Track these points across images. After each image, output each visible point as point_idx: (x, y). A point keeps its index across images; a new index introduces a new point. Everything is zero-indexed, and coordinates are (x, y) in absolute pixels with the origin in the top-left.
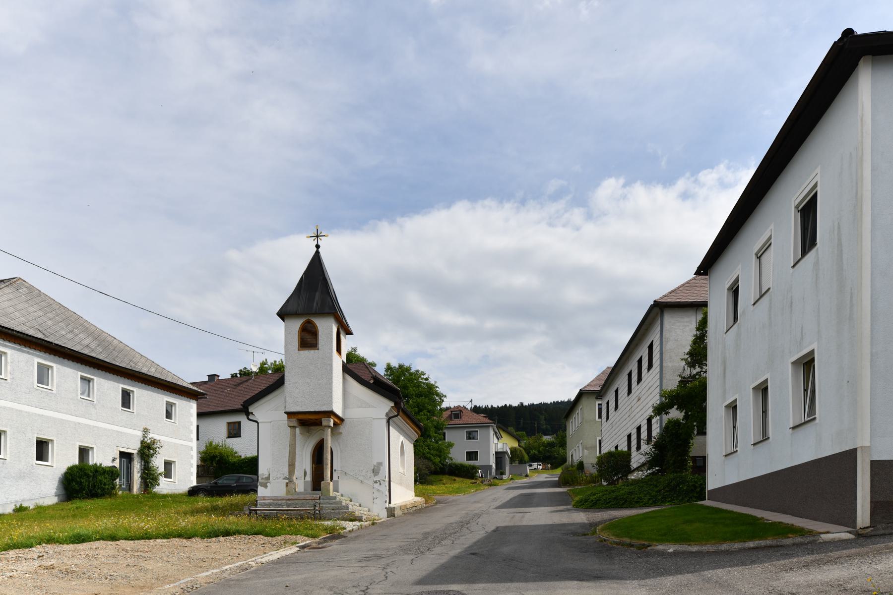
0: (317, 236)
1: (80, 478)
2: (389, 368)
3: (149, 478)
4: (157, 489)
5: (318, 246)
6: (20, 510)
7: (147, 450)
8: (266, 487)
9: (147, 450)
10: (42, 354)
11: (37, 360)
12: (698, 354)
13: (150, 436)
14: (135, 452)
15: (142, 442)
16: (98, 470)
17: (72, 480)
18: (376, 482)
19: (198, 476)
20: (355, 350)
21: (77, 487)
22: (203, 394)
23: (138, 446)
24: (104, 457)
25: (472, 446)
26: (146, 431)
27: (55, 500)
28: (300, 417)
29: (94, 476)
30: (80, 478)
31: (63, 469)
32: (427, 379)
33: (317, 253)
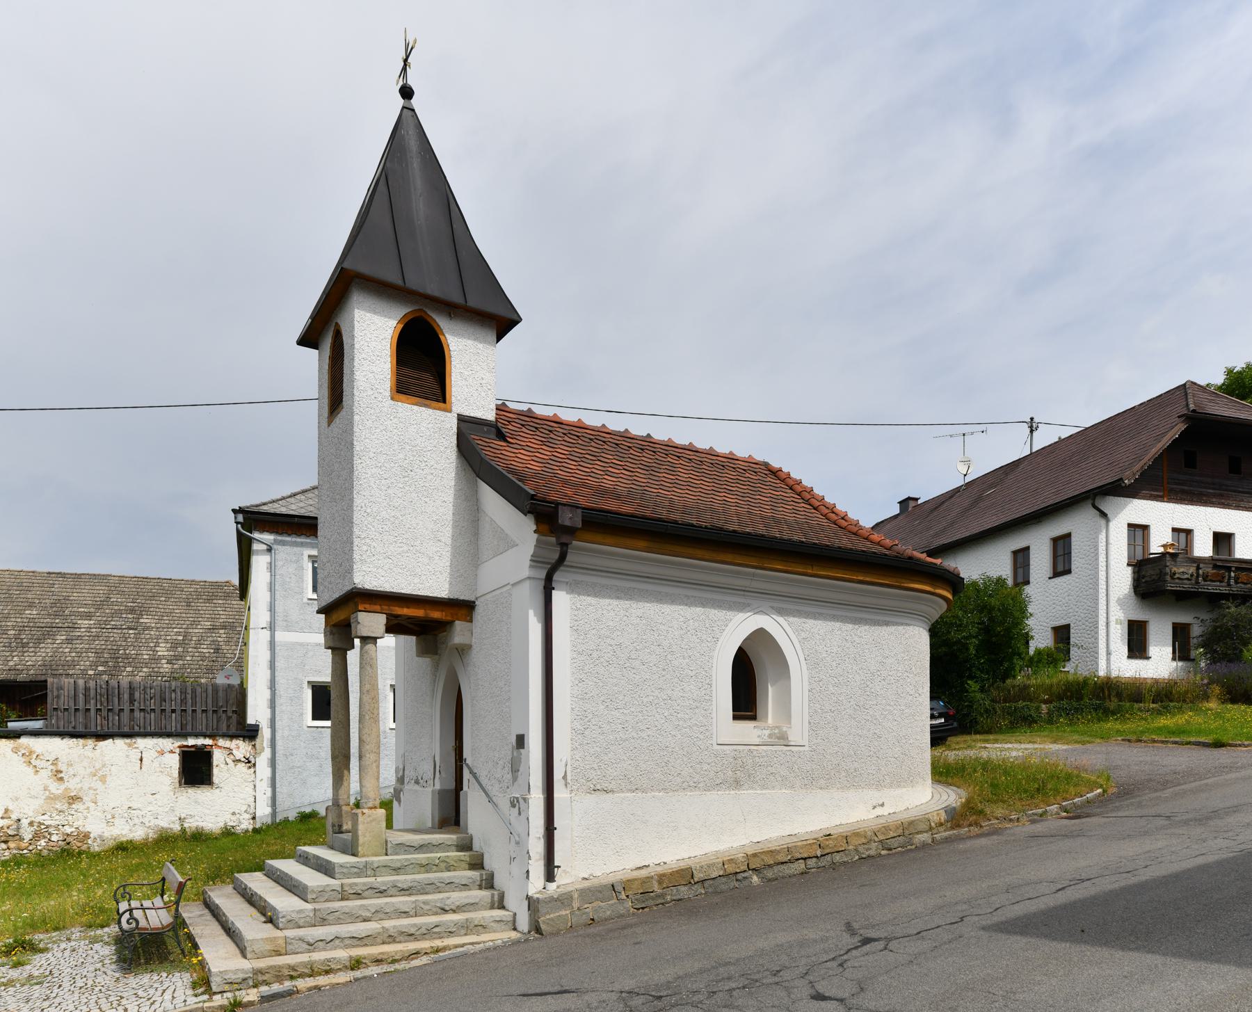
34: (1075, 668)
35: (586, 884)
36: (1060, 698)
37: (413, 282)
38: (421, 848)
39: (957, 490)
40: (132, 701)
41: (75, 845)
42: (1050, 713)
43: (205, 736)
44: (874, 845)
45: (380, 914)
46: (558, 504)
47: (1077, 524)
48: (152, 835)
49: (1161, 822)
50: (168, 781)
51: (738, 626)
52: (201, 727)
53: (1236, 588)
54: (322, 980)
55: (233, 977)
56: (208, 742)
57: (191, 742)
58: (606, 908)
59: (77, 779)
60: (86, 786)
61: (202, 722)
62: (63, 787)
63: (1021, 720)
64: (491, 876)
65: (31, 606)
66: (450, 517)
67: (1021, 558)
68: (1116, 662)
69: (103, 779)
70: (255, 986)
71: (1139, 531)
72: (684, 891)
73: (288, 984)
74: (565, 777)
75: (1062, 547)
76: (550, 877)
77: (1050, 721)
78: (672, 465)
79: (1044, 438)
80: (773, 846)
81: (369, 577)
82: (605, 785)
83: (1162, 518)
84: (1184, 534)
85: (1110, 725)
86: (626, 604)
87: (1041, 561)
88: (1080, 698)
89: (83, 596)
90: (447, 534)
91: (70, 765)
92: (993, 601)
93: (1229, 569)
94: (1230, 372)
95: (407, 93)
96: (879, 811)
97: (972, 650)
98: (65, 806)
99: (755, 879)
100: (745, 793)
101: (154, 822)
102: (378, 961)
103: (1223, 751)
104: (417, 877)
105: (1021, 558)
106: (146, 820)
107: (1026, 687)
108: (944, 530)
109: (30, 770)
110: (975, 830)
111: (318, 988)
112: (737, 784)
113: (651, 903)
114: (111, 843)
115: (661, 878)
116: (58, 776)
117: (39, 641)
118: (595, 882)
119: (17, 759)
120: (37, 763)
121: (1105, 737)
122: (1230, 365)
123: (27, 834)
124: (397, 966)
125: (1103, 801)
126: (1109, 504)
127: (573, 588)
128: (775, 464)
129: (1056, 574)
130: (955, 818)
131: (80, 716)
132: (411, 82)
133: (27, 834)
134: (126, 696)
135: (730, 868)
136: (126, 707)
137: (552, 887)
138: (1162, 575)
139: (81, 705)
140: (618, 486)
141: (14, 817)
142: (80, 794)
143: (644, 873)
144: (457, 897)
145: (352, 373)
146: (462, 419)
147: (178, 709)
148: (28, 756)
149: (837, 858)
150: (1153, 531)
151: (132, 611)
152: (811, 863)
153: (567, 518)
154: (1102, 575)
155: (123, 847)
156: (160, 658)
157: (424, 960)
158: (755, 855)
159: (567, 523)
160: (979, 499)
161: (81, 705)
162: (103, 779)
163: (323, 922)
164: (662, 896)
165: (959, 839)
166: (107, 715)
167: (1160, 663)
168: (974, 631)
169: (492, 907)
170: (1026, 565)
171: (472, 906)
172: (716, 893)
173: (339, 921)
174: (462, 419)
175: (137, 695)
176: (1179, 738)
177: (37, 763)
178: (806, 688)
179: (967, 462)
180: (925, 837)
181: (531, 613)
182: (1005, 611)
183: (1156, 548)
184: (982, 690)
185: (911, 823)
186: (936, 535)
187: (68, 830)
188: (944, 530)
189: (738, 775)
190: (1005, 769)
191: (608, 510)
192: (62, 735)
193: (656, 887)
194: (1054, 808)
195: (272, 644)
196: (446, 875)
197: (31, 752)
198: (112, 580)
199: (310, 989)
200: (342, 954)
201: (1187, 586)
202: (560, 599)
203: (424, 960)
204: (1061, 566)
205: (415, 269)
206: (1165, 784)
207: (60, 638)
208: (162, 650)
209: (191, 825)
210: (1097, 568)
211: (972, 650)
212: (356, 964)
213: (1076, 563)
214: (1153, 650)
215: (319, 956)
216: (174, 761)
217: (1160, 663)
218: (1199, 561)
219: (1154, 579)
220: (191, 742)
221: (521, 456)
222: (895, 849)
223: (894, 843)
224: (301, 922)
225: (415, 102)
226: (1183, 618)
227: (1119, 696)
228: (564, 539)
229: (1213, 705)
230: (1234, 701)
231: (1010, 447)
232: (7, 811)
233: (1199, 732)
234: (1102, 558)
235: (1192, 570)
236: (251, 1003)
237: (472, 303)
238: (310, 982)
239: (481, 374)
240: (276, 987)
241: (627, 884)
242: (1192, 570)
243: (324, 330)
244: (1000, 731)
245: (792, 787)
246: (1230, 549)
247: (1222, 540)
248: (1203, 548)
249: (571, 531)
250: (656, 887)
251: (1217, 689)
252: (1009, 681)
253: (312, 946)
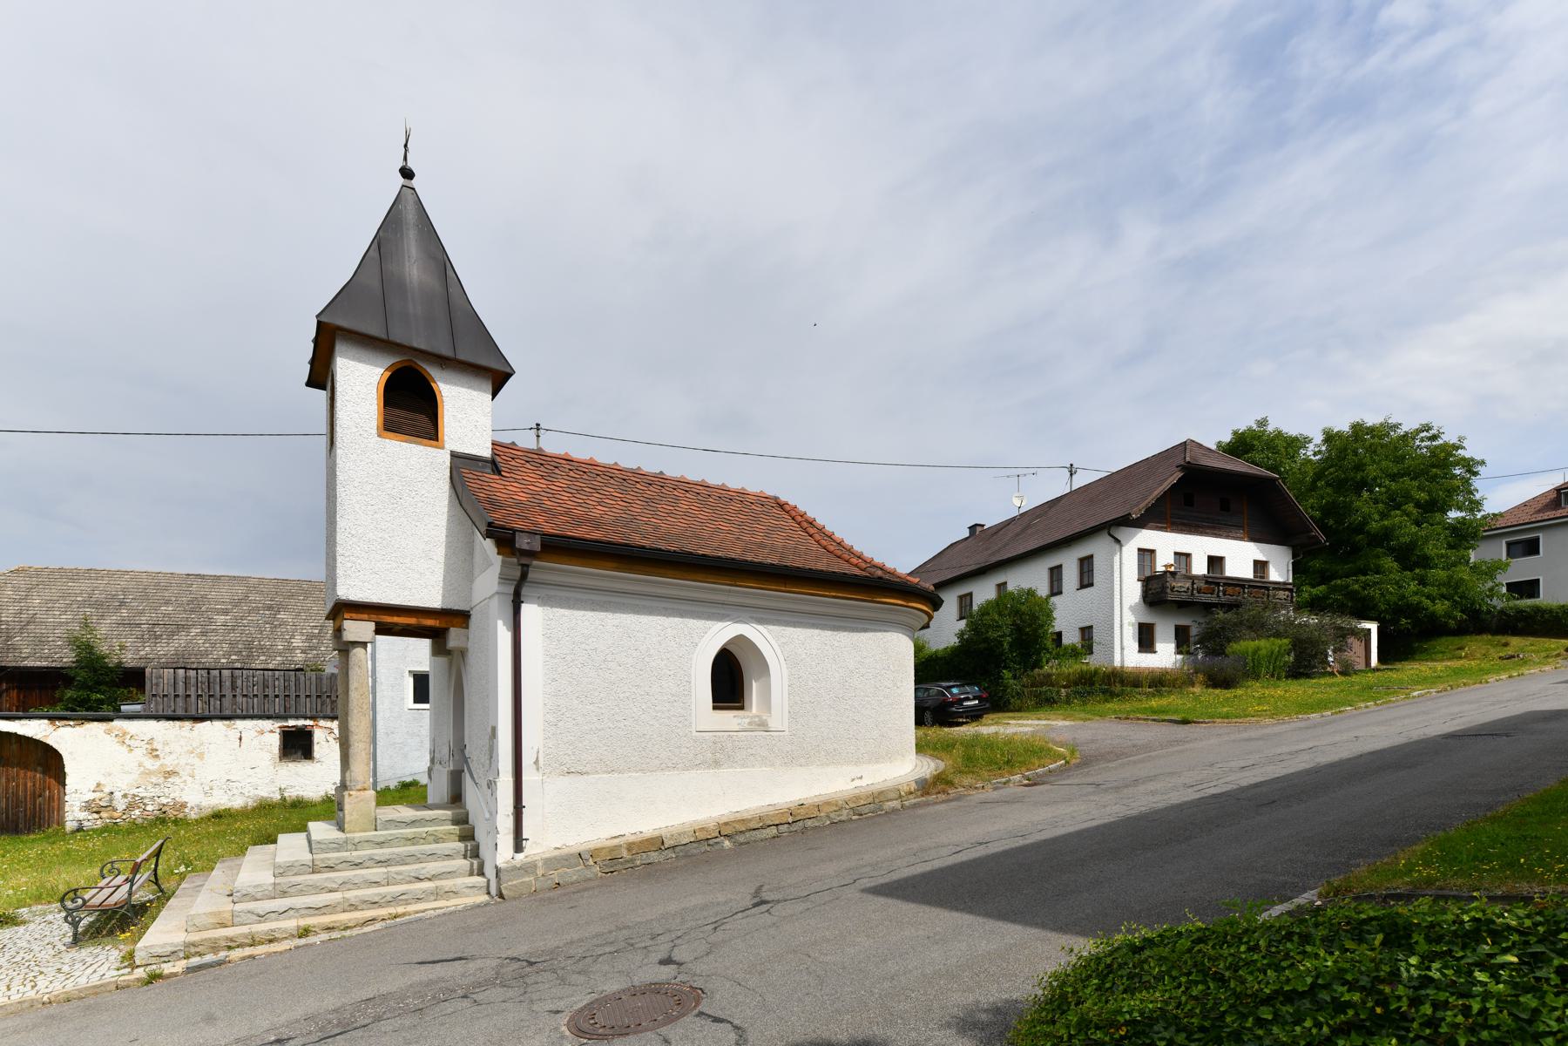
2: (1330, 437)
25: (1522, 569)
32: (1434, 438)
34: (1094, 661)
35: (557, 853)
36: (1076, 684)
37: (397, 336)
38: (413, 823)
39: (1013, 519)
40: (234, 687)
41: (171, 813)
42: (1068, 696)
43: (306, 718)
44: (845, 812)
45: (344, 884)
46: (514, 531)
47: (1097, 548)
48: (251, 804)
49: (1090, 789)
50: (268, 756)
51: (718, 633)
52: (302, 711)
53: (1224, 599)
54: (260, 950)
55: (160, 951)
56: (308, 722)
57: (291, 723)
58: (572, 874)
59: (173, 757)
60: (183, 761)
61: (307, 705)
63: (1044, 701)
64: (478, 847)
65: (167, 603)
66: (443, 538)
67: (1056, 573)
68: (1128, 656)
69: (201, 756)
70: (187, 957)
71: (1146, 554)
72: (654, 856)
73: (222, 954)
74: (536, 762)
75: (1086, 564)
76: (518, 847)
77: (1068, 702)
78: (677, 498)
79: (1080, 481)
80: (746, 816)
81: (350, 590)
82: (579, 768)
83: (1166, 545)
84: (1186, 557)
85: (1113, 705)
86: (602, 615)
87: (1070, 576)
88: (1092, 684)
89: (224, 594)
90: (440, 553)
91: (166, 744)
92: (1023, 608)
93: (1218, 584)
94: (1235, 433)
95: (407, 173)
96: (857, 783)
97: (1006, 645)
98: (161, 780)
99: (727, 843)
100: (725, 772)
101: (253, 793)
102: (329, 929)
103: (1187, 727)
104: (396, 850)
105: (1056, 573)
106: (245, 791)
107: (1049, 675)
108: (998, 551)
109: (124, 749)
110: (942, 797)
111: (253, 957)
112: (717, 764)
113: (619, 867)
114: (208, 812)
115: (630, 846)
116: (153, 753)
117: (173, 633)
118: (565, 851)
120: (132, 742)
121: (1102, 715)
122: (1328, 425)
123: (120, 805)
124: (348, 933)
125: (1066, 770)
126: (1122, 533)
127: (545, 601)
128: (783, 498)
129: (1083, 586)
130: (927, 787)
131: (180, 702)
132: (410, 164)
133: (120, 805)
134: (228, 684)
135: (701, 836)
136: (228, 692)
137: (520, 856)
138: (1164, 588)
139: (181, 691)
140: (604, 518)
141: (107, 790)
143: (616, 842)
144: (433, 867)
146: (454, 455)
147: (314, 694)
148: (122, 738)
149: (809, 823)
150: (1158, 554)
151: (270, 608)
152: (783, 828)
153: (523, 542)
154: (1117, 588)
155: (218, 816)
156: (295, 648)
157: (378, 926)
158: (726, 824)
159: (525, 547)
160: (1028, 526)
161: (181, 691)
162: (201, 756)
163: (284, 894)
164: (632, 861)
165: (927, 804)
166: (207, 697)
167: (1165, 656)
168: (1007, 631)
169: (471, 874)
170: (1060, 580)
171: (450, 874)
172: (686, 856)
173: (301, 893)
174: (454, 455)
175: (239, 682)
176: (1158, 716)
177: (132, 742)
178: (786, 683)
179: (1021, 498)
180: (896, 804)
181: (500, 623)
182: (1034, 618)
183: (1160, 568)
184: (1015, 677)
185: (881, 793)
186: (993, 554)
187: (164, 801)
188: (998, 551)
189: (717, 756)
190: (989, 744)
191: (563, 535)
192: (157, 718)
193: (625, 854)
194: (1018, 777)
196: (433, 847)
197: (125, 734)
198: (252, 582)
199: (243, 959)
200: (291, 924)
201: (1184, 597)
202: (529, 611)
203: (378, 926)
204: (1086, 582)
205: (407, 331)
206: (1118, 757)
207: (194, 631)
208: (297, 642)
209: (291, 794)
210: (1112, 582)
211: (1006, 645)
212: (305, 932)
213: (1098, 577)
214: (1159, 646)
215: (262, 928)
216: (275, 740)
217: (1165, 656)
218: (1193, 578)
219: (1158, 591)
220: (291, 723)
221: (511, 490)
222: (868, 815)
223: (865, 810)
224: (259, 896)
225: (415, 183)
226: (1184, 621)
227: (1122, 682)
228: (525, 561)
229: (1197, 690)
230: (1215, 686)
231: (1057, 487)
232: (98, 785)
233: (1176, 712)
234: (1117, 575)
235: (1188, 585)
236: (175, 975)
237: (461, 357)
238: (248, 951)
239: (469, 419)
240: (209, 958)
241: (594, 853)
242: (1188, 585)
243: (321, 376)
244: (1027, 710)
245: (772, 765)
246: (1222, 569)
247: (1215, 562)
248: (1200, 568)
249: (531, 554)
250: (625, 854)
251: (1201, 677)
252: (1036, 670)
253: (262, 917)
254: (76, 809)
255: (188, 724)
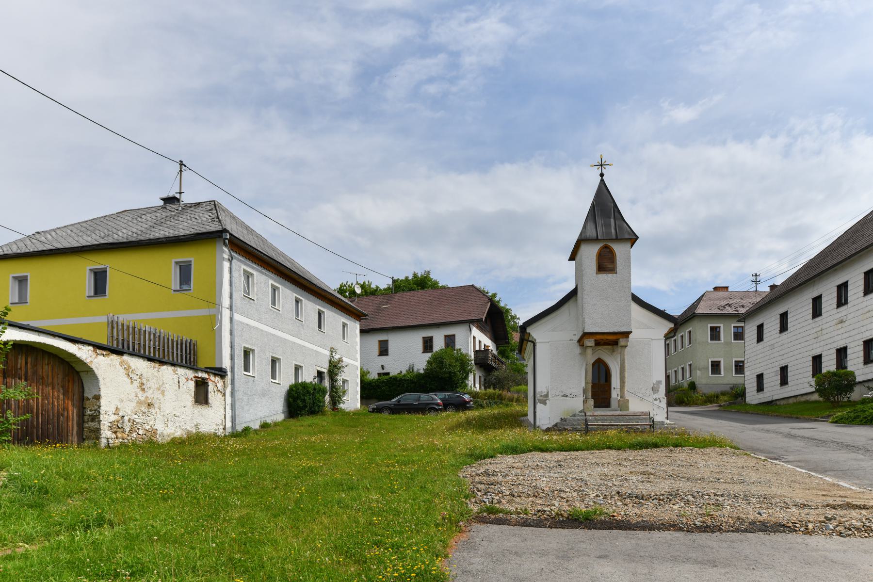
0: (601, 165)
1: (304, 395)
3: (336, 399)
4: (341, 406)
5: (602, 175)
6: (264, 426)
7: (334, 368)
8: (545, 404)
9: (334, 368)
10: (275, 277)
11: (271, 282)
12: (431, 80)
13: (337, 357)
14: (325, 371)
15: (330, 362)
16: (304, 385)
17: (298, 398)
18: (656, 400)
19: (362, 397)
20: (428, 273)
21: (301, 404)
22: (366, 315)
23: (327, 365)
24: (308, 377)
26: (332, 350)
27: (280, 417)
28: (598, 337)
29: (313, 394)
30: (304, 395)
31: (287, 388)
33: (602, 180)
59: (151, 391)
62: (144, 395)
75: (784, 317)
91: (148, 380)
109: (129, 381)
119: (122, 371)
141: (121, 414)
142: (153, 402)
145: (266, 275)
148: (128, 371)
187: (148, 427)
195: (231, 319)
216: (192, 385)
220: (200, 374)
254: (106, 428)
255: (157, 365)
